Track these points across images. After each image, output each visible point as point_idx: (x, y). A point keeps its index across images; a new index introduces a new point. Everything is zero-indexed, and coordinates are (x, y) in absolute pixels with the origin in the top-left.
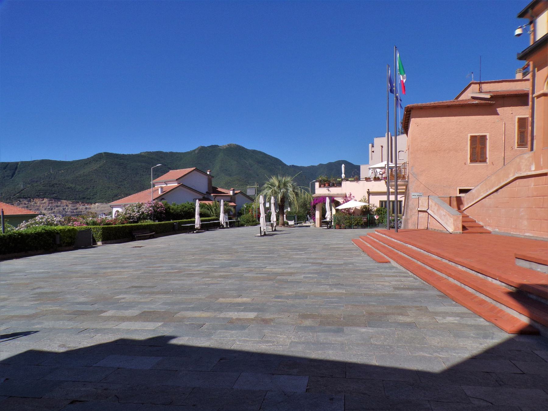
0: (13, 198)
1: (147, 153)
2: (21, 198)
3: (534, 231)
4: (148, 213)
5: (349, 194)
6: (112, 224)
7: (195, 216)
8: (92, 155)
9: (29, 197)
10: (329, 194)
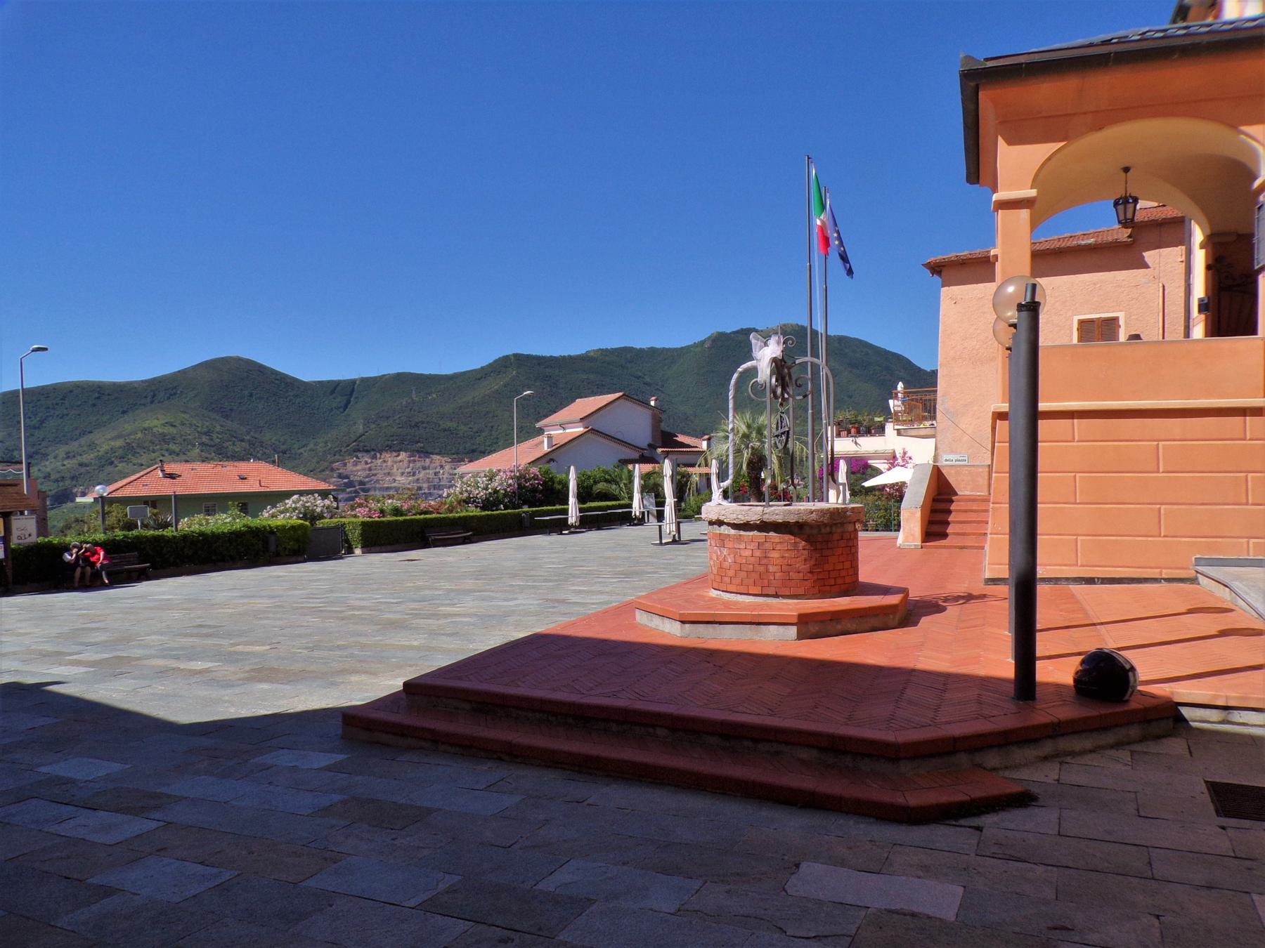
0: (345, 452)
1: (600, 352)
2: (359, 451)
4: (505, 490)
5: (902, 452)
6: (431, 513)
9: (373, 450)
10: (858, 451)
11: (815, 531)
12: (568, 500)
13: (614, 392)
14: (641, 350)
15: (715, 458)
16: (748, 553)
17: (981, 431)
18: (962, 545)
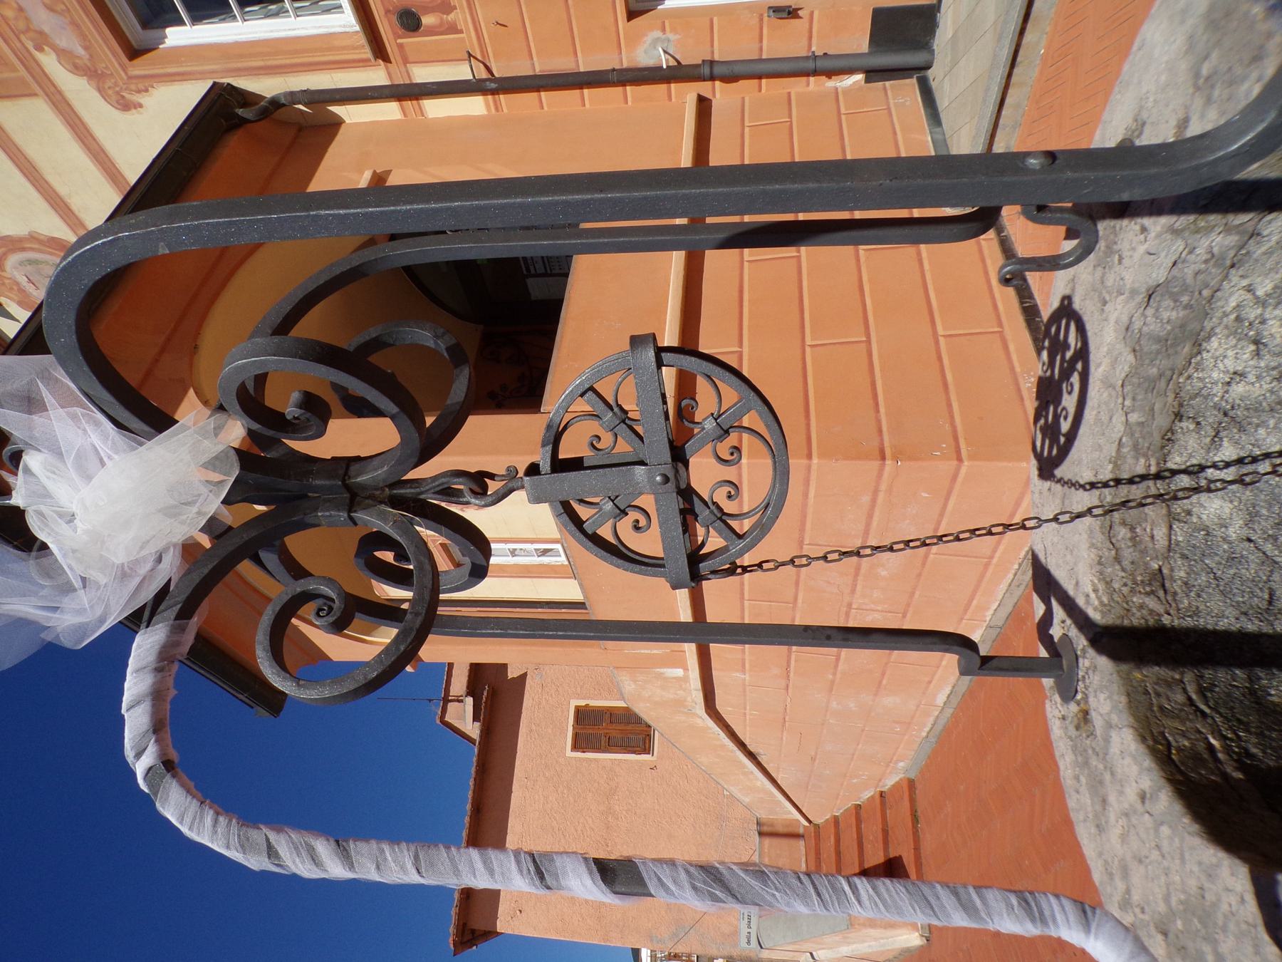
3: (930, 682)
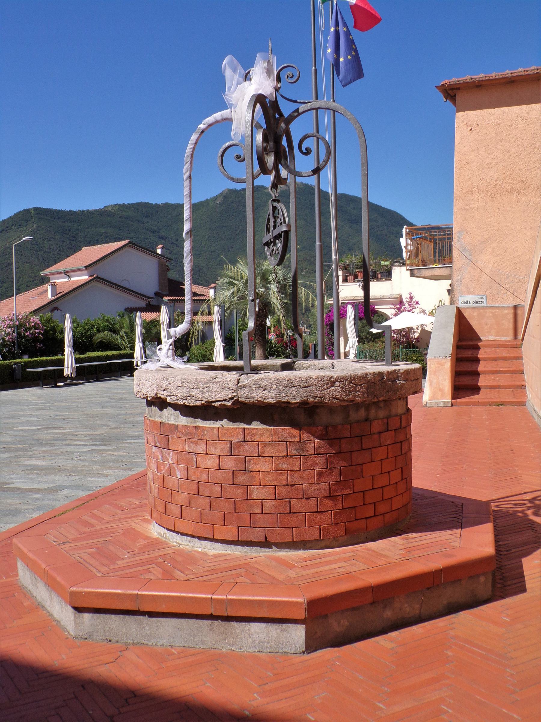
1: (117, 208)
5: (409, 296)
7: (64, 350)
8: (12, 214)
11: (338, 419)
12: (63, 350)
13: (120, 240)
14: (157, 205)
15: (217, 305)
16: (211, 462)
17: (500, 270)
18: (499, 400)
